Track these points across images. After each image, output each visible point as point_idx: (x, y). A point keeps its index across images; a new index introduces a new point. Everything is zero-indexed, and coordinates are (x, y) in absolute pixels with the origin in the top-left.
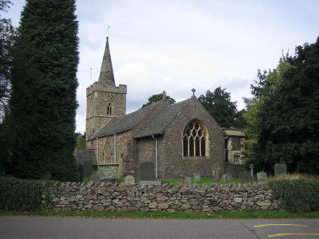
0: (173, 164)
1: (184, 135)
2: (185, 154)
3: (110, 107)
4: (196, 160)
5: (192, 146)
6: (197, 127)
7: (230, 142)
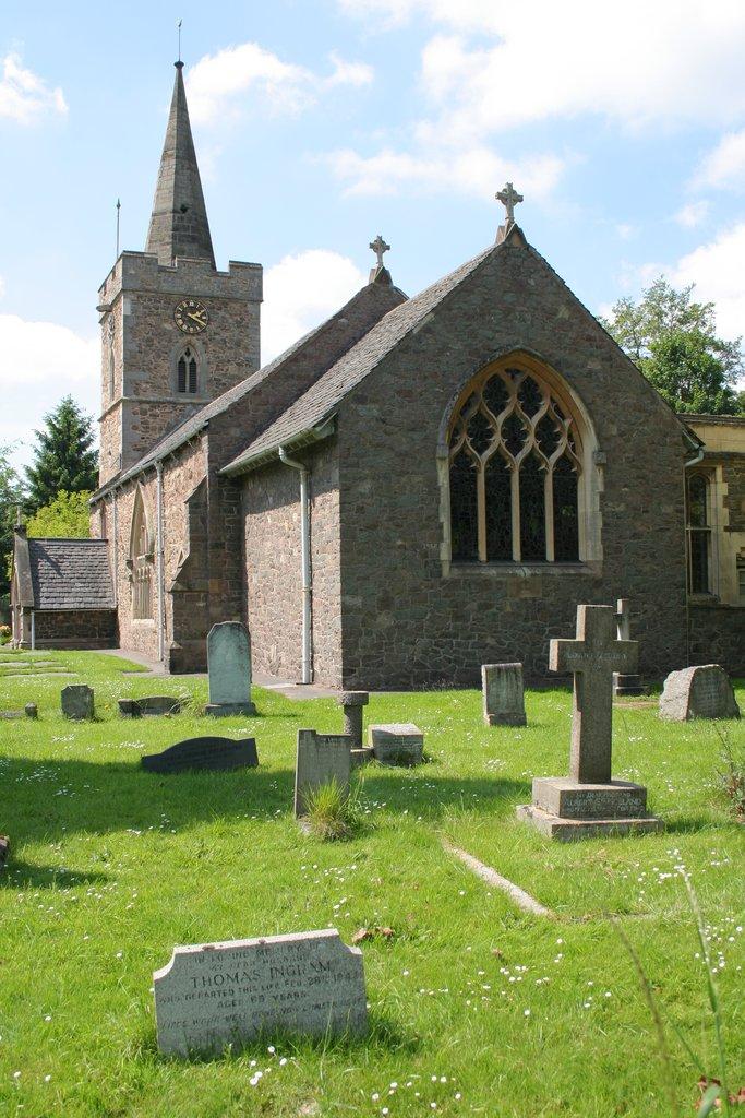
0: (386, 603)
1: (453, 443)
2: (464, 552)
3: (188, 360)
4: (522, 584)
5: (499, 503)
6: (530, 398)
7: (719, 489)
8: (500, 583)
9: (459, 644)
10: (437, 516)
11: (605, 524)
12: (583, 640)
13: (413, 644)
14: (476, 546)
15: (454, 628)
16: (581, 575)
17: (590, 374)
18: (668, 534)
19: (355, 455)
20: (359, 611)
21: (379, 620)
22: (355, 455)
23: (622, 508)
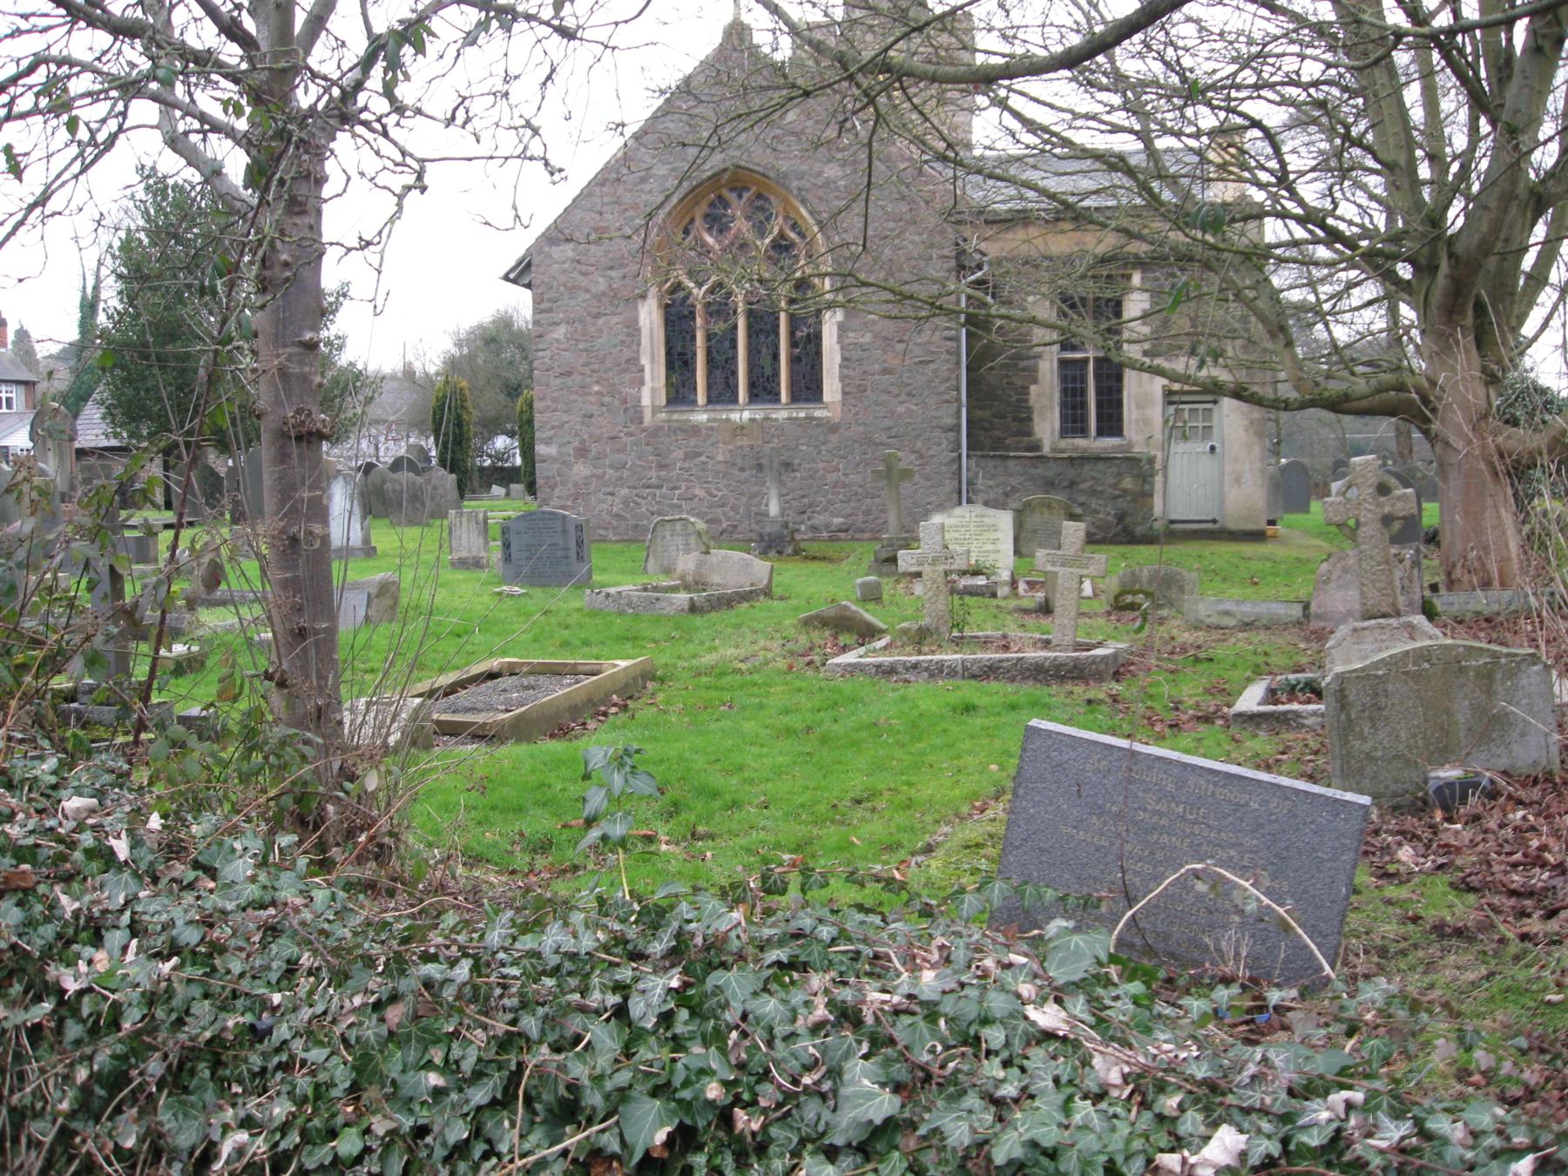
0: (582, 452)
2: (679, 393)
8: (712, 428)
9: (663, 496)
10: (637, 359)
11: (844, 359)
12: (1004, 521)
13: (612, 494)
14: (695, 388)
15: (658, 477)
16: (813, 418)
17: (827, 183)
18: (933, 366)
19: (550, 300)
20: (555, 460)
21: (575, 468)
22: (550, 300)
23: (868, 338)
